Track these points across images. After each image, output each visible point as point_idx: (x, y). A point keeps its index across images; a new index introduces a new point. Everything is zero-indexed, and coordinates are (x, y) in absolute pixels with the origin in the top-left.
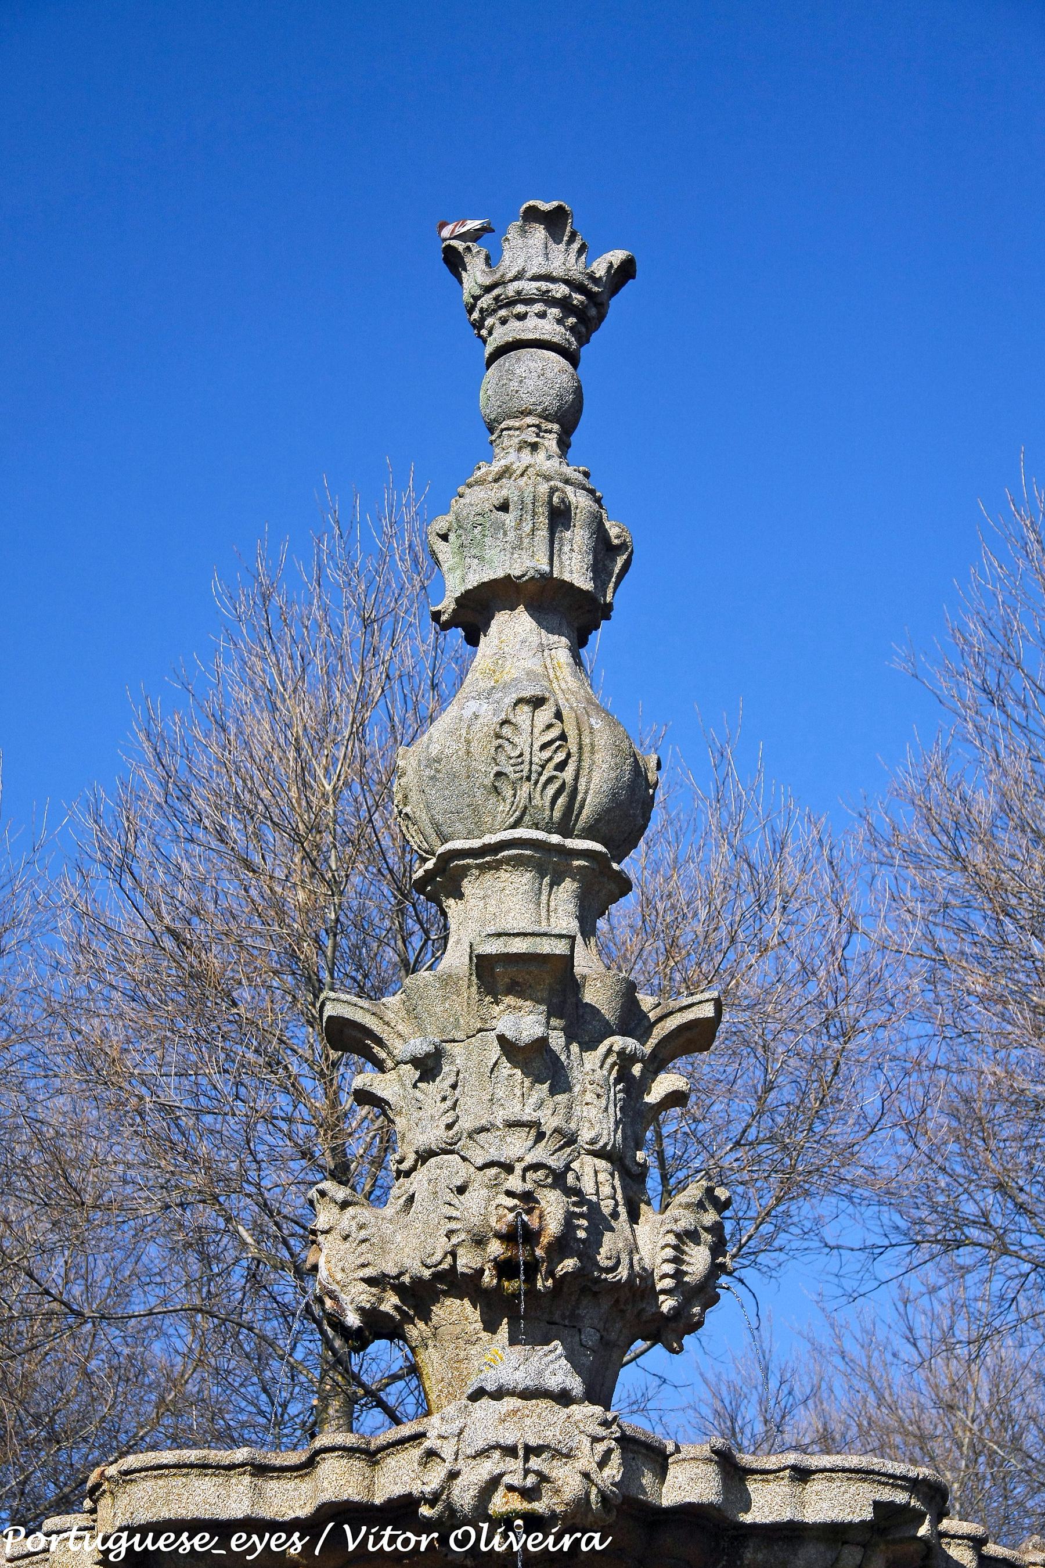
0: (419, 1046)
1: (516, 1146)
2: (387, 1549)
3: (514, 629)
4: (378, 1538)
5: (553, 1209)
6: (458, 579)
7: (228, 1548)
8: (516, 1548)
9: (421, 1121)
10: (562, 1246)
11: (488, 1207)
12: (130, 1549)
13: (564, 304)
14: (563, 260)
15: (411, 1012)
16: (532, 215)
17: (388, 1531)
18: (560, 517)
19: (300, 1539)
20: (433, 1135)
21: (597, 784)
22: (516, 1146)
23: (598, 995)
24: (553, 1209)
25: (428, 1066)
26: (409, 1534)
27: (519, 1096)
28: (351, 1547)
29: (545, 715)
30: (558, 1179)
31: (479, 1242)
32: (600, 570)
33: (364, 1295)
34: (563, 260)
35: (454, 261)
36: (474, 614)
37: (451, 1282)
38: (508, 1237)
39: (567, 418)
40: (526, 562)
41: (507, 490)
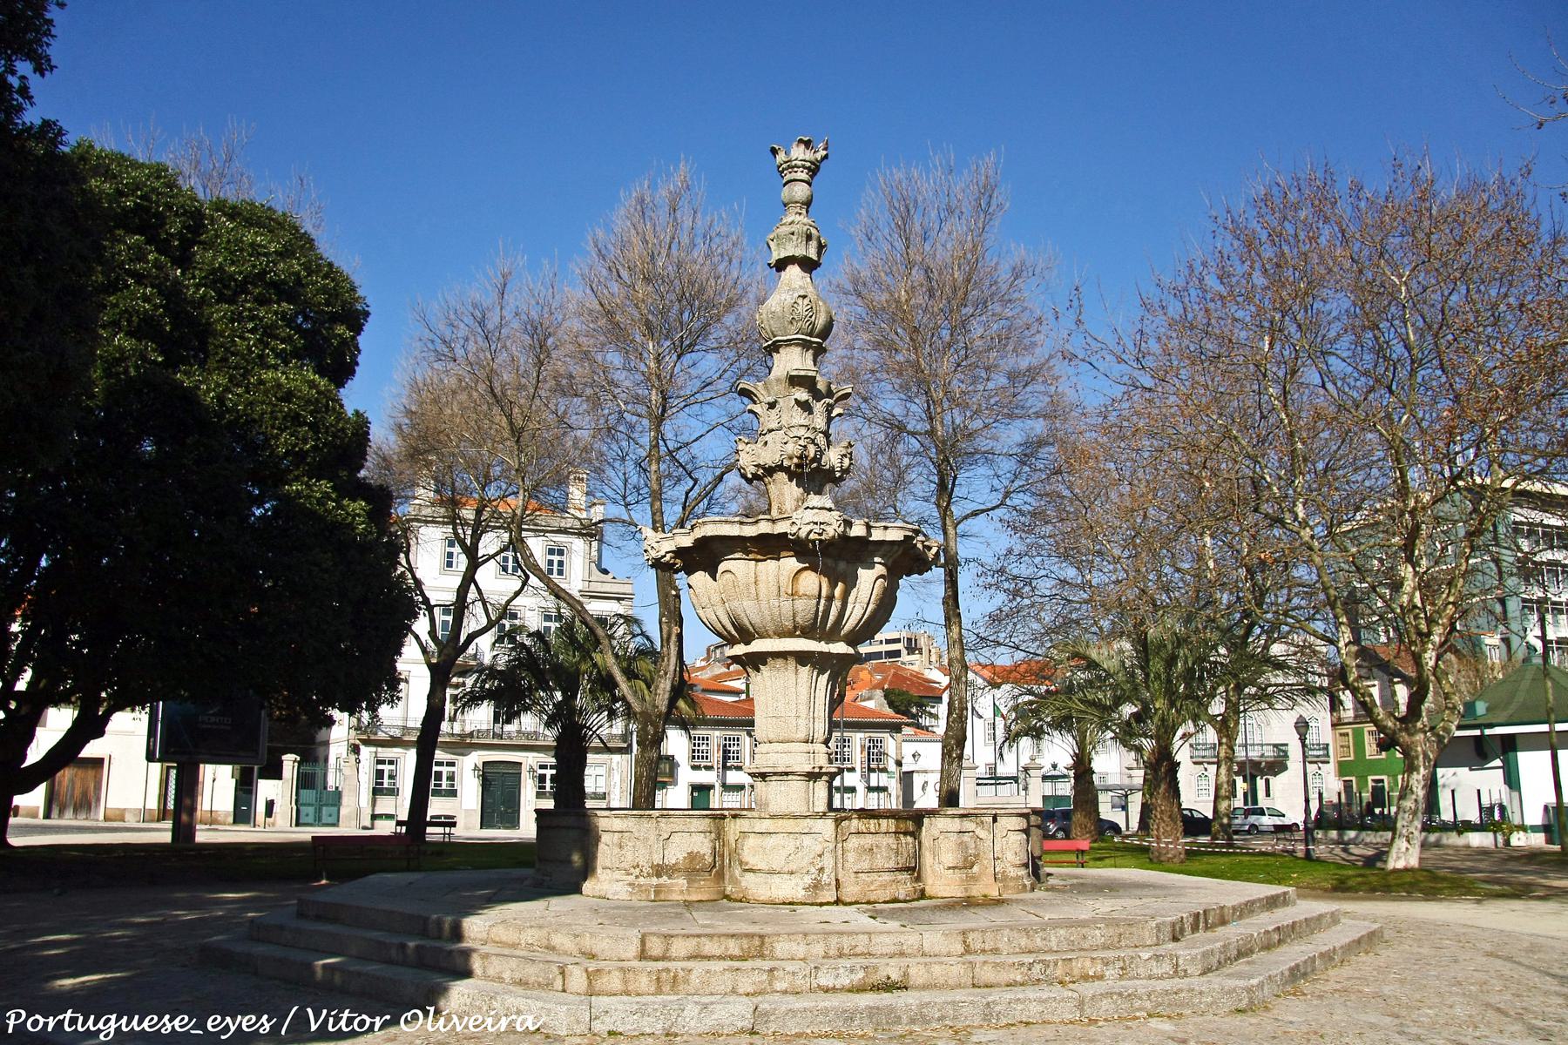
0: (771, 399)
1: (802, 432)
2: (345, 1029)
3: (794, 271)
4: (337, 1020)
5: (812, 450)
6: (777, 254)
7: (204, 1028)
8: (459, 1029)
9: (770, 419)
10: (814, 460)
11: (793, 448)
12: (118, 1029)
13: (809, 169)
14: (809, 155)
15: (766, 388)
16: (801, 141)
17: (346, 1014)
18: (809, 237)
19: (269, 1021)
20: (774, 425)
21: (821, 321)
22: (802, 432)
23: (821, 386)
24: (812, 450)
25: (772, 406)
26: (364, 1017)
27: (799, 417)
28: (314, 1028)
29: (806, 301)
30: (813, 441)
31: (791, 458)
32: (819, 254)
33: (753, 469)
34: (809, 155)
35: (774, 152)
36: (781, 265)
37: (780, 468)
38: (800, 458)
39: (808, 204)
40: (799, 251)
41: (794, 228)
